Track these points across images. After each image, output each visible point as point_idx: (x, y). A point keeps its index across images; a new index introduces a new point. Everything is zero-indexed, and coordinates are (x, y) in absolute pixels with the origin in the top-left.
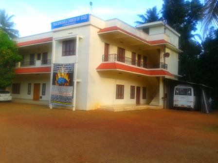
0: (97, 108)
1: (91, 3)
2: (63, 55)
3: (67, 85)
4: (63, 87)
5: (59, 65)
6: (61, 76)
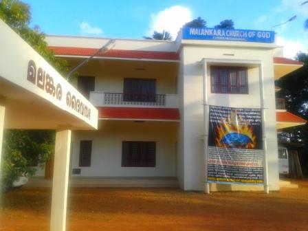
3: (250, 148)
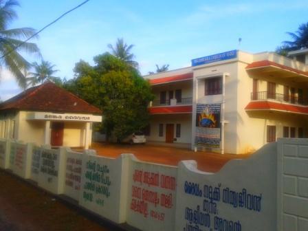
1: (240, 40)
2: (206, 95)
3: (213, 127)
5: (203, 105)
6: (205, 116)
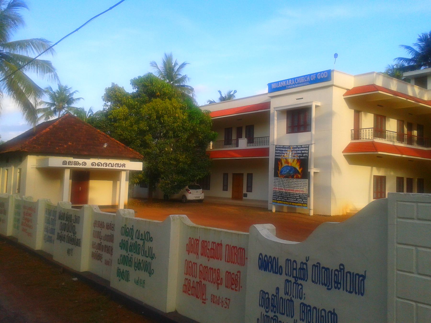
0: (345, 214)
1: (336, 56)
3: (297, 178)
4: (291, 180)
5: (284, 147)
